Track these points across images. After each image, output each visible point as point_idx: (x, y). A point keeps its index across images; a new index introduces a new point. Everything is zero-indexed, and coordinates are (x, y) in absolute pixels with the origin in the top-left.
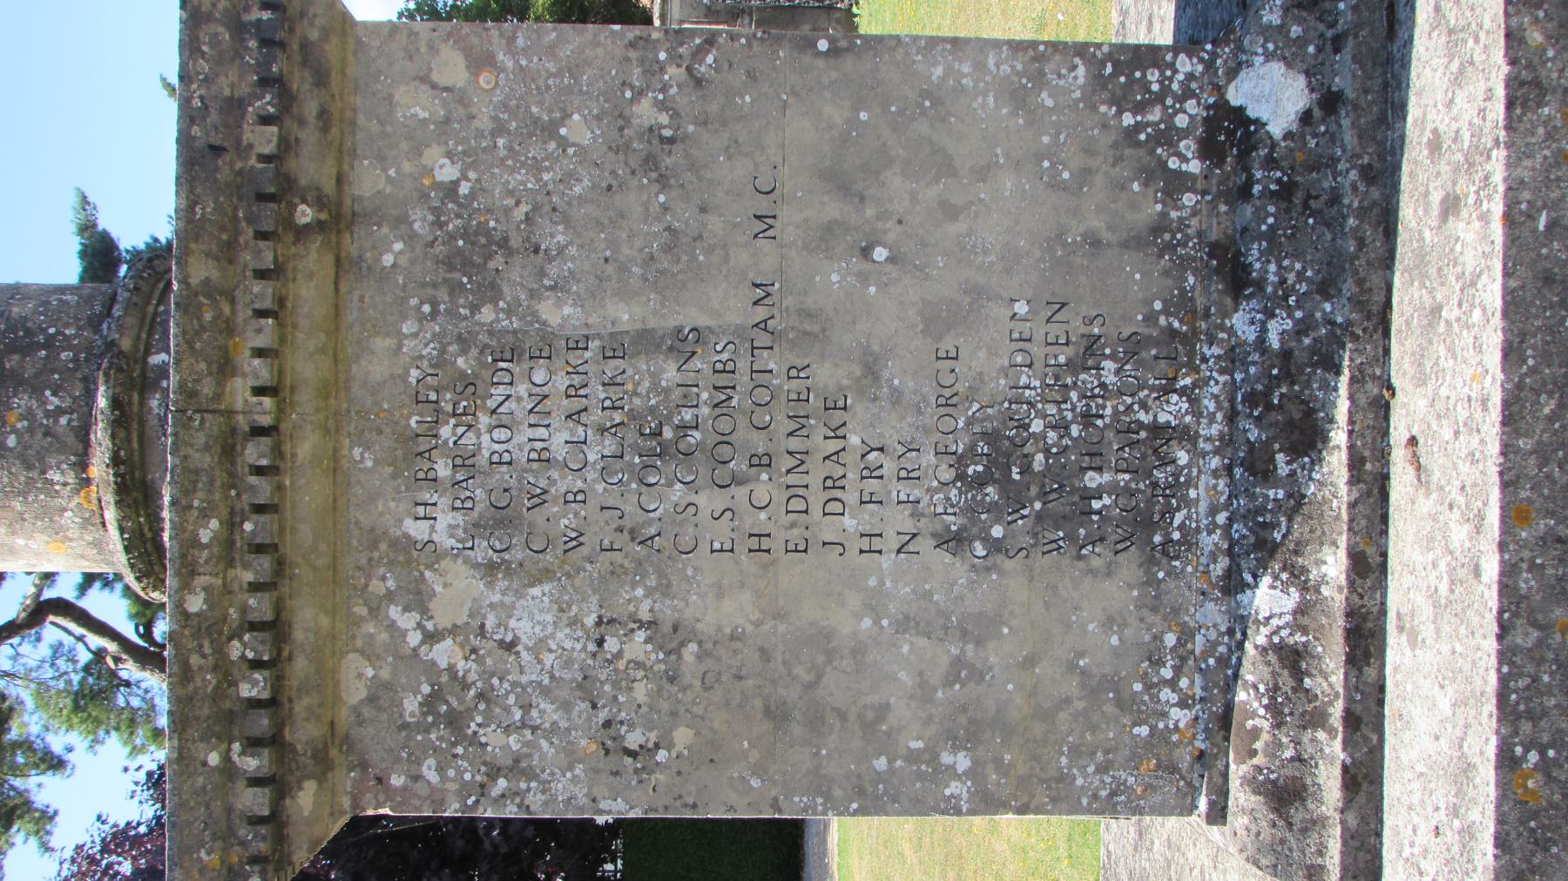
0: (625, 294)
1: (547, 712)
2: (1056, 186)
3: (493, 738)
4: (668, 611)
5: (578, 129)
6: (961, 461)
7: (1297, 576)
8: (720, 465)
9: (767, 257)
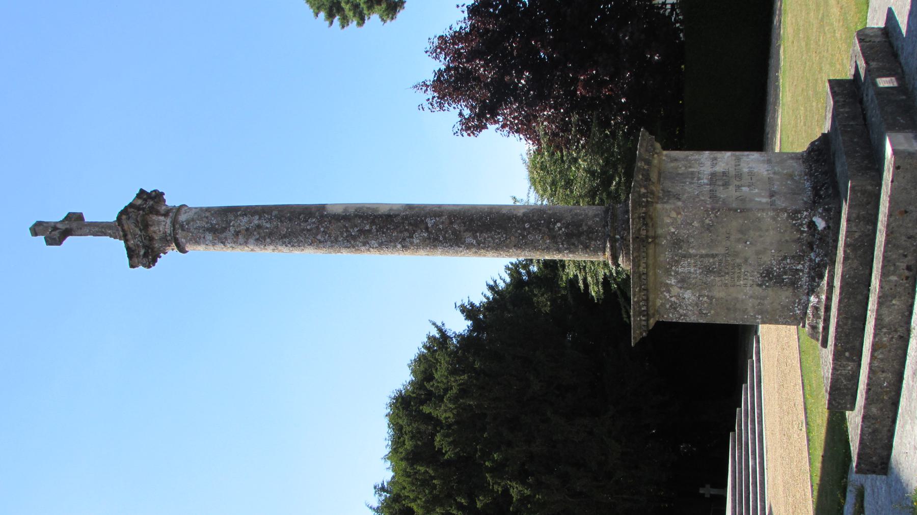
0: (704, 249)
1: (690, 308)
2: (780, 232)
3: (681, 311)
4: (710, 294)
5: (696, 224)
6: (761, 274)
7: (818, 297)
8: (719, 273)
9: (729, 243)
